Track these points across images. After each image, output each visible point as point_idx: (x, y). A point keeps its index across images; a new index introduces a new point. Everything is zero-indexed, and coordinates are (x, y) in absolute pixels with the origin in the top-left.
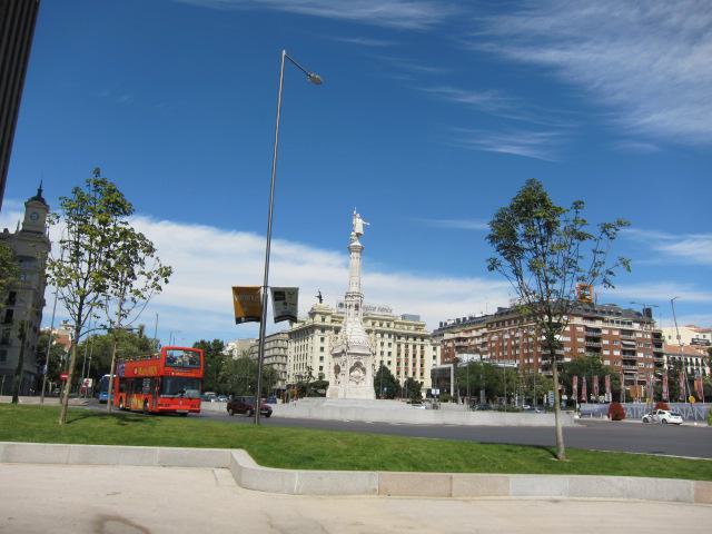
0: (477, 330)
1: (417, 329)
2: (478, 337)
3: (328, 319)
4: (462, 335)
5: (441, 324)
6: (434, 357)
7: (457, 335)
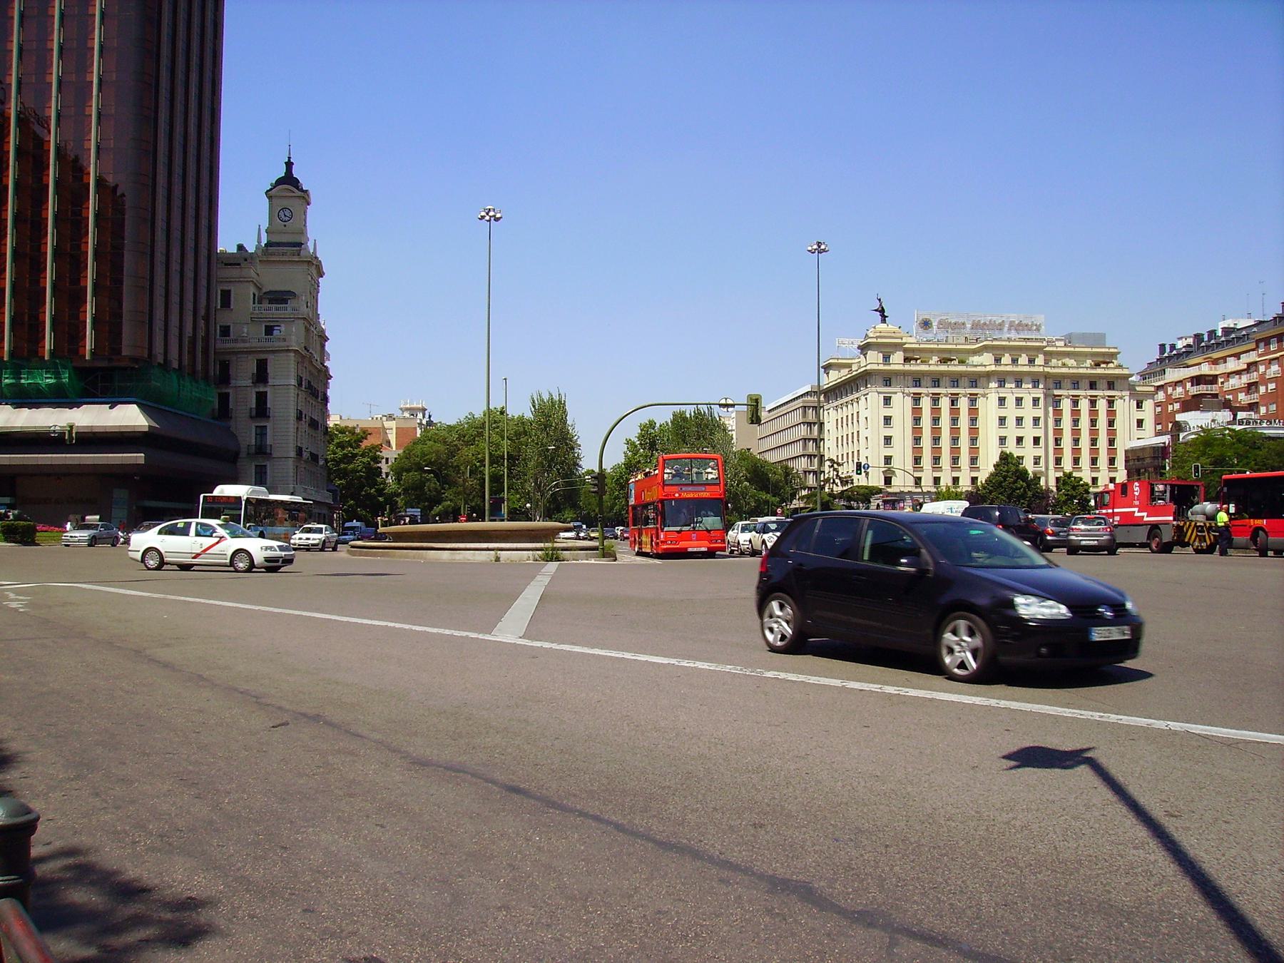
0: (1237, 356)
1: (1097, 365)
2: (1239, 373)
3: (897, 357)
4: (1206, 369)
5: (1162, 347)
6: (1140, 423)
7: (1194, 372)
